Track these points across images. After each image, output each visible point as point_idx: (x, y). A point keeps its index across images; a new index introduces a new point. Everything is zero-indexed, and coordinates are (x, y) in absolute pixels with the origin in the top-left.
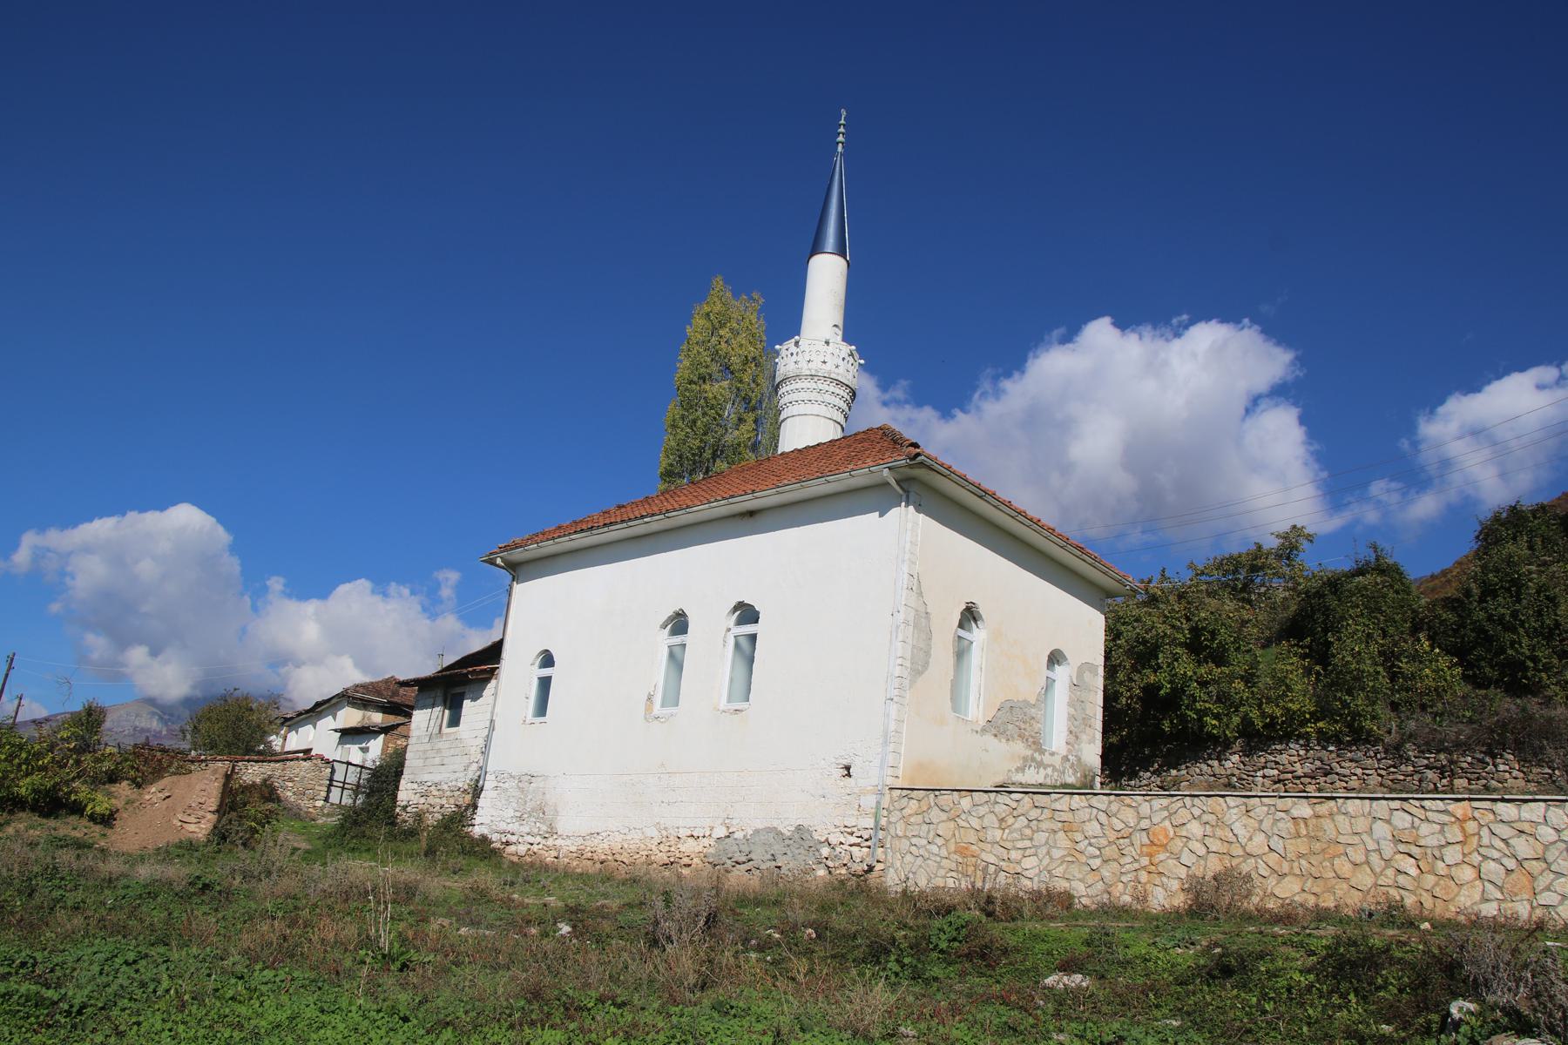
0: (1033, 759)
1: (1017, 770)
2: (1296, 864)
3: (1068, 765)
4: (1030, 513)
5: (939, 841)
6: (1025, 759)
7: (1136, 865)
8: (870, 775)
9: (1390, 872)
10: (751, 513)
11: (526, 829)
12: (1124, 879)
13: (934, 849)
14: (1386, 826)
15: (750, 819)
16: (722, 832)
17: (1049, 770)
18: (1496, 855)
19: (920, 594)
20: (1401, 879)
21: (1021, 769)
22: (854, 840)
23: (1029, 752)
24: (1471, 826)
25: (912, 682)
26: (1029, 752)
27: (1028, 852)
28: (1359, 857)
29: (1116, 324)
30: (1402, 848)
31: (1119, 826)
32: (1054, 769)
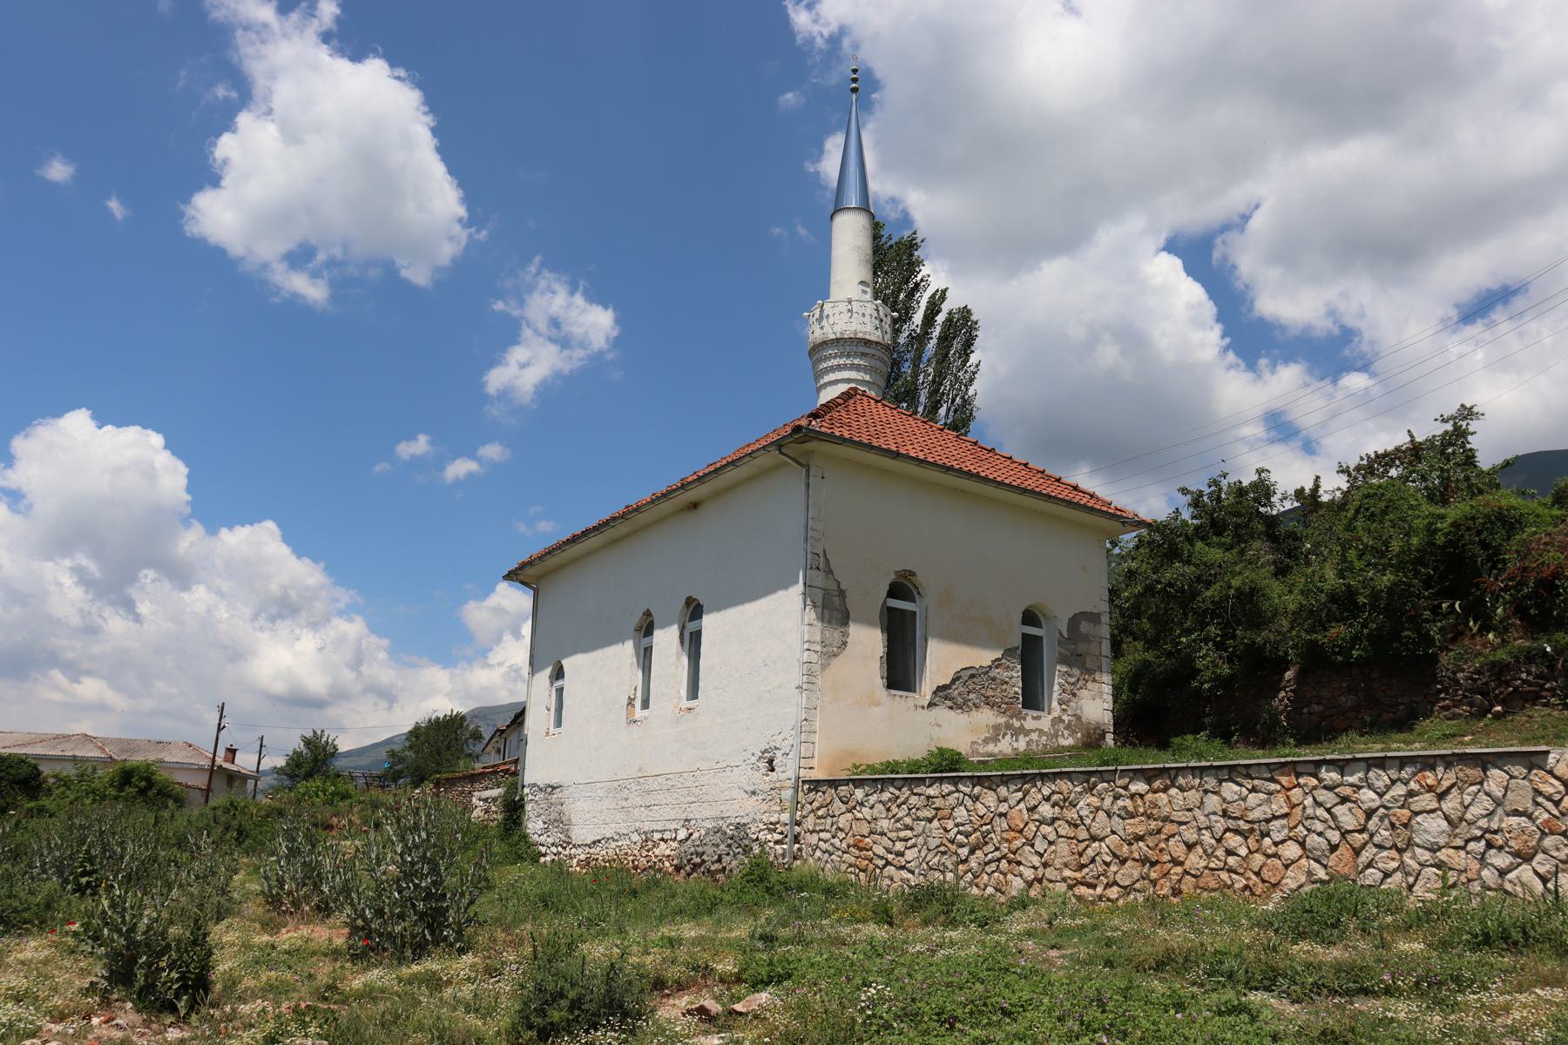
0: (1008, 726)
1: (986, 741)
2: (1135, 847)
3: (1061, 726)
4: (590, 525)
5: (841, 835)
6: (996, 728)
7: (997, 854)
8: (787, 770)
9: (1220, 853)
10: (695, 506)
11: (550, 840)
12: (988, 869)
13: (836, 841)
14: (1215, 797)
15: (705, 816)
16: (682, 834)
17: (1034, 736)
18: (1319, 827)
19: (829, 572)
20: (1231, 860)
21: (995, 739)
22: (777, 837)
23: (1002, 720)
24: (1296, 794)
25: (824, 667)
26: (1002, 720)
27: (910, 843)
28: (1191, 836)
29: (94, 417)
30: (1231, 824)
31: (982, 811)
32: (1041, 732)
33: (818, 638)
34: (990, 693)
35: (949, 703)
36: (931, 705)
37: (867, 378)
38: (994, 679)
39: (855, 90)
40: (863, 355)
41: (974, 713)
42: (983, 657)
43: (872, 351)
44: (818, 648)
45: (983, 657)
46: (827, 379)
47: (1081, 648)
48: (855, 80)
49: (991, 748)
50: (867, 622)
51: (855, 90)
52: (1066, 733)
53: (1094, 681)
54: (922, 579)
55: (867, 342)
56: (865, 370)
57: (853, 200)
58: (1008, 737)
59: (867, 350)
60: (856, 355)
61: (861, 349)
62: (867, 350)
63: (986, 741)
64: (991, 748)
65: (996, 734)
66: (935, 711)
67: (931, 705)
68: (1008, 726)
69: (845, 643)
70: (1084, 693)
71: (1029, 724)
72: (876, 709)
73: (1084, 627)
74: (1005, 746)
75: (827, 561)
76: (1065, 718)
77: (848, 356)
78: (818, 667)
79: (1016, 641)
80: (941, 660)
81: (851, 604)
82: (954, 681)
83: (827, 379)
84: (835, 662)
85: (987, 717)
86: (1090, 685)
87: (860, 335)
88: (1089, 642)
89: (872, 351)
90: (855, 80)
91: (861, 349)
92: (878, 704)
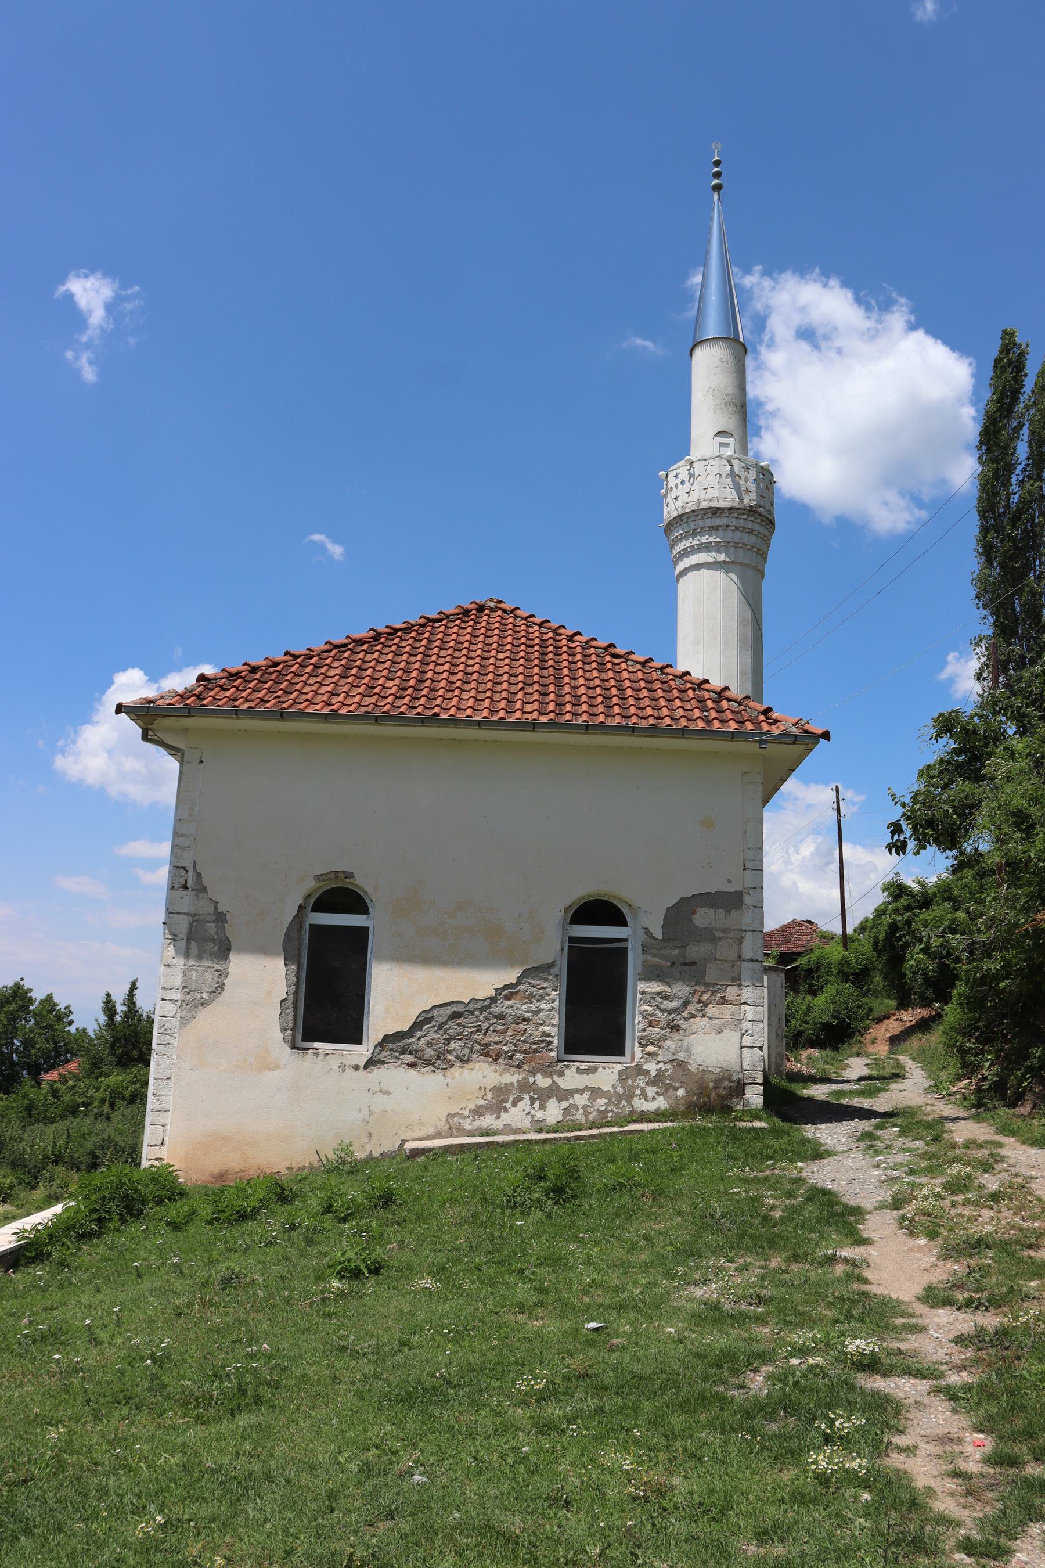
1: (478, 1112)
3: (641, 1081)
21: (498, 1108)
23: (513, 1078)
25: (185, 1021)
33: (178, 982)
34: (492, 1037)
35: (408, 1058)
36: (370, 1063)
37: (722, 557)
38: (501, 1017)
39: (717, 188)
40: (713, 529)
41: (456, 1071)
42: (481, 983)
43: (725, 521)
44: (177, 996)
45: (481, 983)
46: (682, 565)
47: (695, 951)
48: (717, 175)
49: (488, 1121)
50: (264, 950)
51: (717, 188)
52: (651, 1091)
53: (724, 1001)
54: (364, 882)
55: (716, 512)
56: (718, 547)
57: (712, 327)
58: (524, 1104)
59: (717, 522)
60: (703, 531)
61: (709, 522)
62: (717, 522)
63: (478, 1112)
64: (488, 1121)
65: (500, 1100)
66: (379, 1073)
67: (370, 1063)
68: (524, 1087)
69: (222, 986)
70: (699, 1023)
71: (570, 1079)
72: (271, 1074)
73: (703, 917)
74: (518, 1119)
75: (199, 876)
76: (652, 1067)
77: (694, 534)
78: (176, 1022)
79: (552, 948)
80: (394, 994)
81: (230, 931)
82: (417, 1025)
83: (682, 565)
84: (203, 1014)
85: (484, 1075)
86: (711, 1010)
87: (704, 505)
88: (714, 940)
89: (725, 521)
90: (717, 175)
91: (709, 522)
92: (276, 1067)
